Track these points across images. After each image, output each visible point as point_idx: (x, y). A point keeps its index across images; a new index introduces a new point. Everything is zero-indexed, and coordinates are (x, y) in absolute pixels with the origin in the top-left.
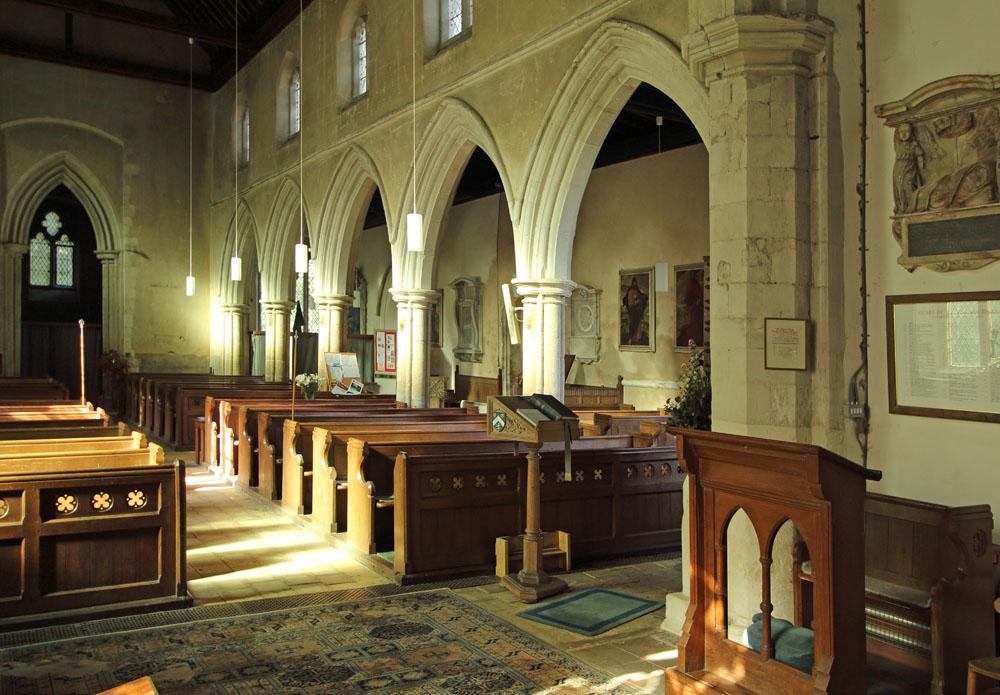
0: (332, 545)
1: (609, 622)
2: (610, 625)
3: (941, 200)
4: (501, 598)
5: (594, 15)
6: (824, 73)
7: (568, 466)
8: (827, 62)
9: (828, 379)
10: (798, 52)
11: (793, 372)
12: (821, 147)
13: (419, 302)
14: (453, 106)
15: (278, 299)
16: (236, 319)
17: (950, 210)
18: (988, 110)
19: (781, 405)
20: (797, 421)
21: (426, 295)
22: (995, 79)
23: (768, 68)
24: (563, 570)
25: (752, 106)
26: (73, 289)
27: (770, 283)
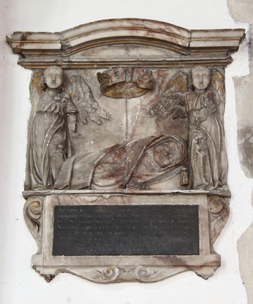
3: (111, 175)
17: (126, 191)
18: (171, 73)
22: (194, 35)
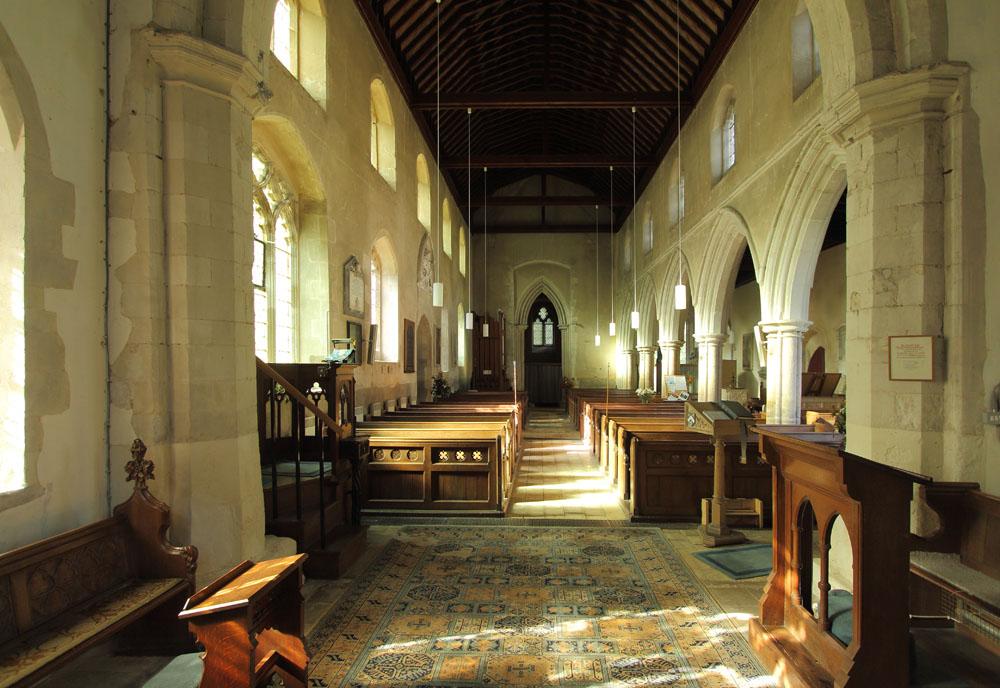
0: (612, 491)
1: (759, 571)
2: (759, 574)
4: (688, 542)
5: (809, 125)
6: (958, 112)
7: (744, 452)
8: (961, 101)
9: (960, 388)
10: (927, 100)
11: (920, 383)
12: (955, 182)
13: (712, 342)
14: (727, 213)
15: (646, 345)
16: (629, 356)
19: (906, 412)
20: (923, 425)
21: (717, 337)
23: (894, 122)
24: (755, 527)
25: (878, 158)
26: (552, 346)
27: (895, 306)
